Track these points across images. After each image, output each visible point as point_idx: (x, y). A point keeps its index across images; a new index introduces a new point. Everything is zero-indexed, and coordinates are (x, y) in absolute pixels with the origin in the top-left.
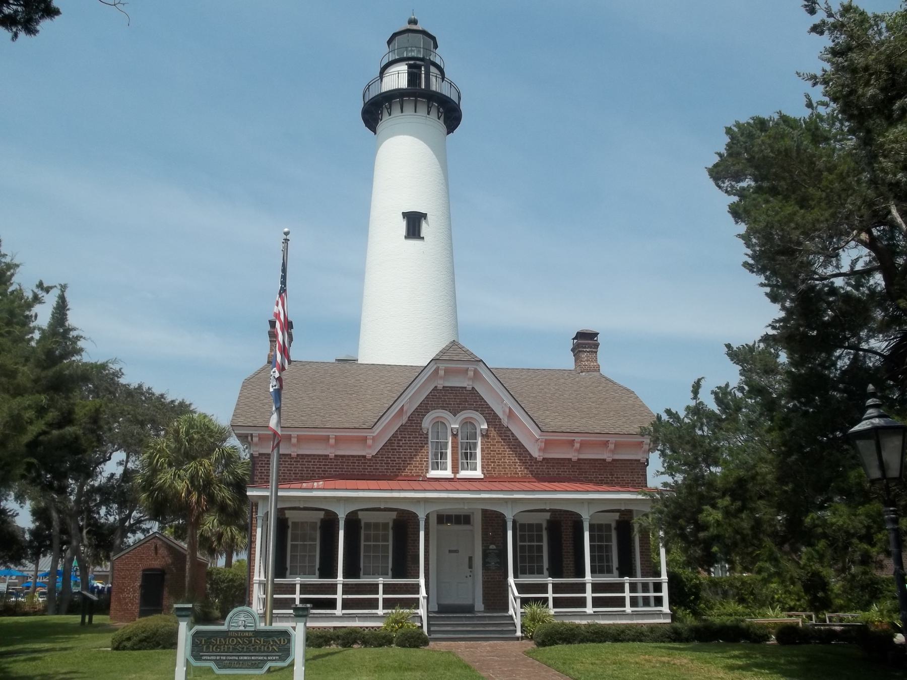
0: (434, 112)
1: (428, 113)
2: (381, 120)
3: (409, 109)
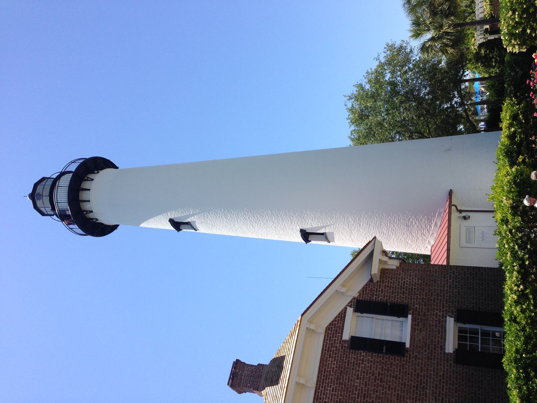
0: (91, 176)
1: (92, 180)
2: (97, 220)
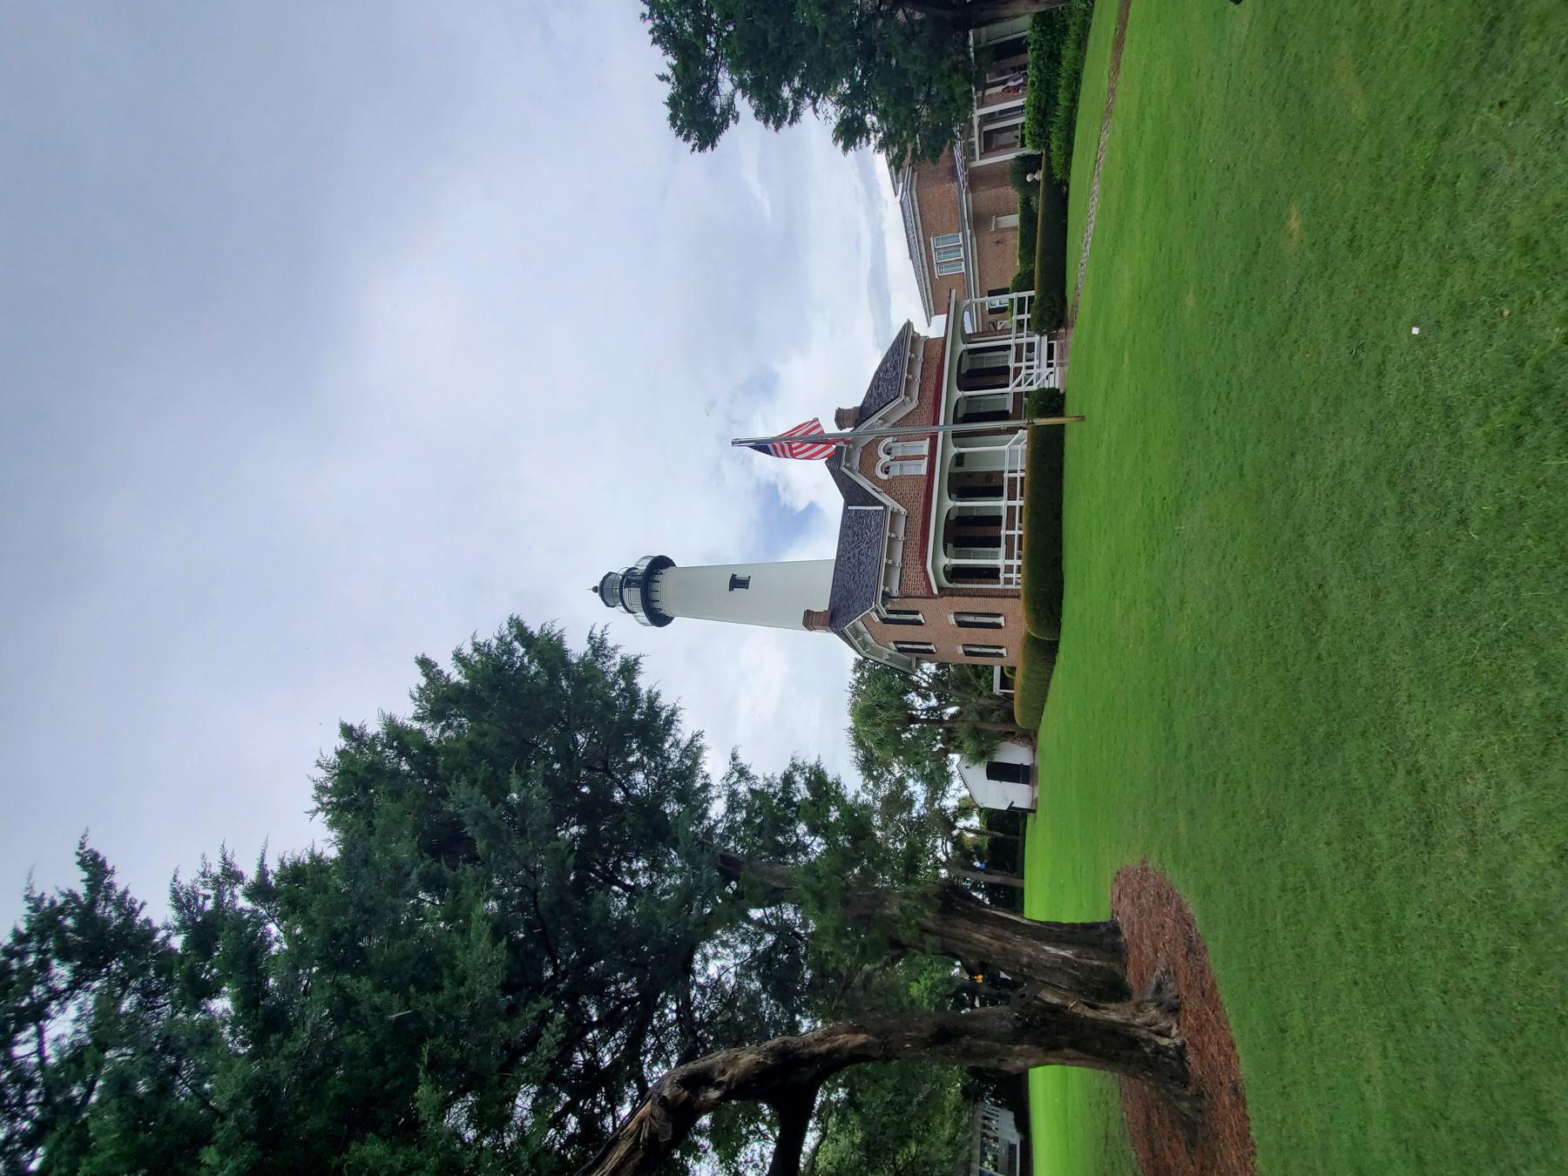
3: (655, 586)
